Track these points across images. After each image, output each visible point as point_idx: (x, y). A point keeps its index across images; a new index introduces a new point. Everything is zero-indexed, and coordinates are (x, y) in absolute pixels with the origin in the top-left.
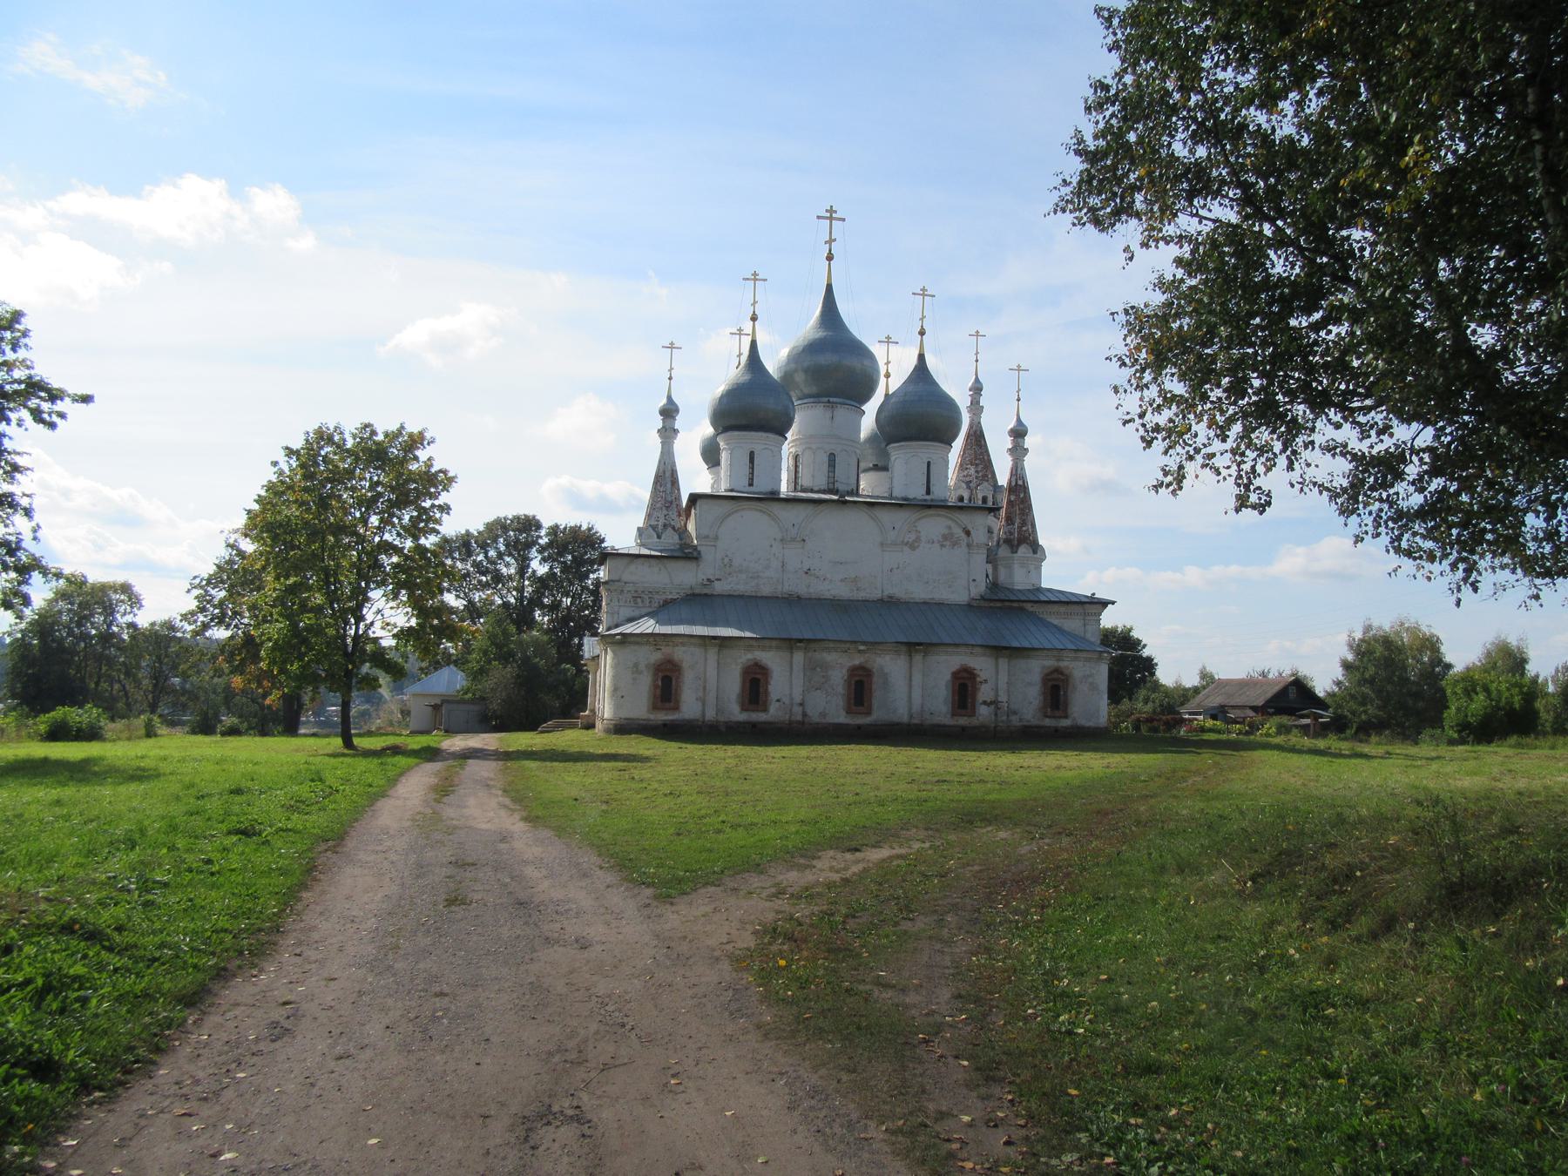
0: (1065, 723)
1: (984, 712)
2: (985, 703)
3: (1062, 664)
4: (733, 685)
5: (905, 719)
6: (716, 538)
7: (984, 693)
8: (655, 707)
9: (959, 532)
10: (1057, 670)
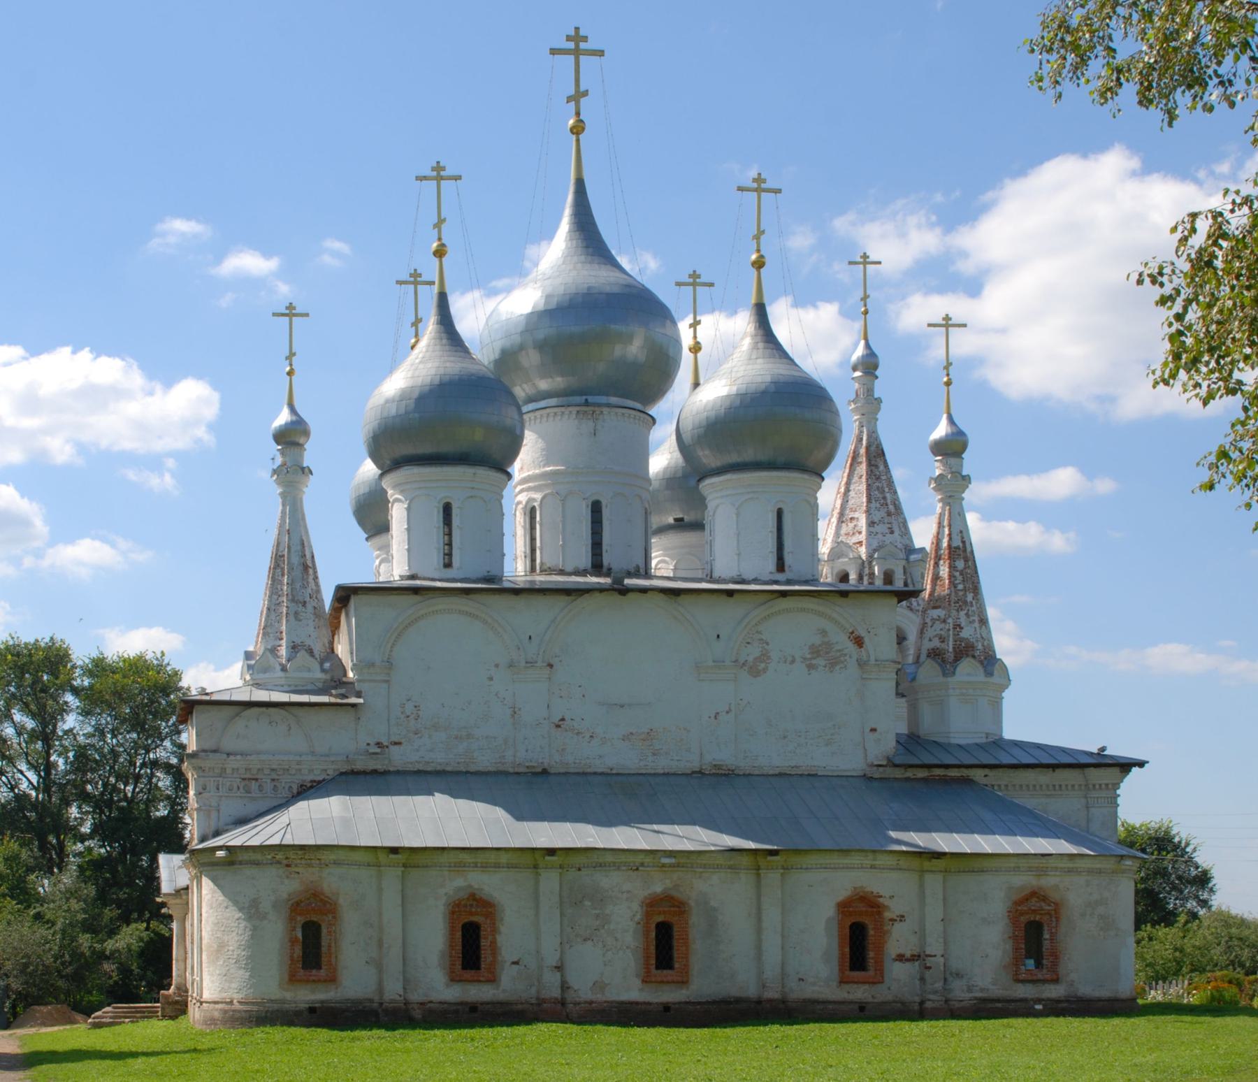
2: (900, 958)
4: (432, 938)
7: (899, 940)
8: (293, 979)
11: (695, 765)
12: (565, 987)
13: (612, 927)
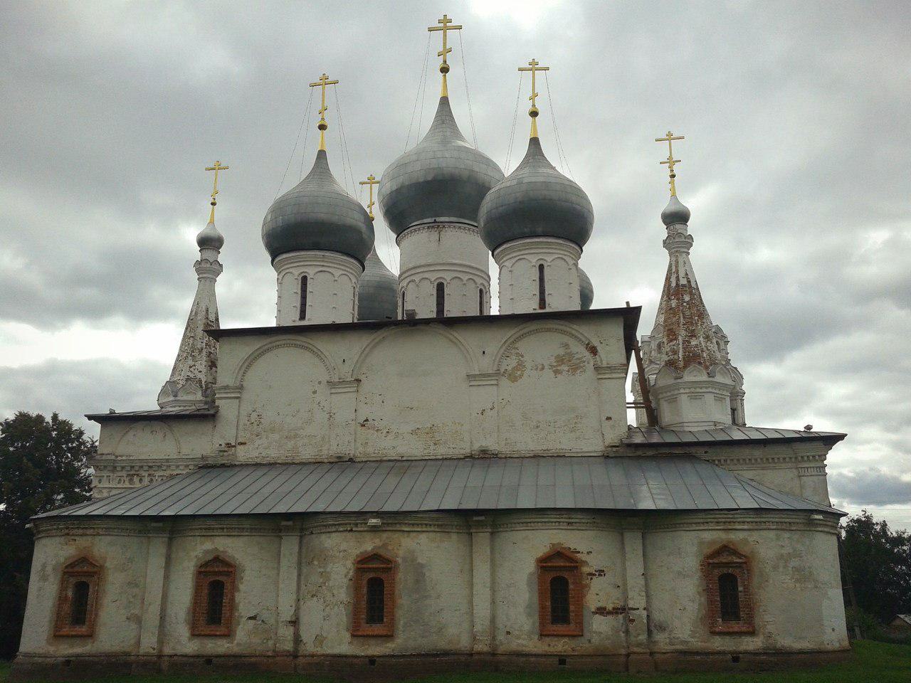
0: (751, 644)
1: (600, 629)
2: (601, 611)
3: (736, 537)
5: (464, 643)
6: (241, 388)
7: (598, 593)
9: (580, 351)
10: (726, 549)
11: (467, 451)
12: (297, 640)
13: (331, 583)
